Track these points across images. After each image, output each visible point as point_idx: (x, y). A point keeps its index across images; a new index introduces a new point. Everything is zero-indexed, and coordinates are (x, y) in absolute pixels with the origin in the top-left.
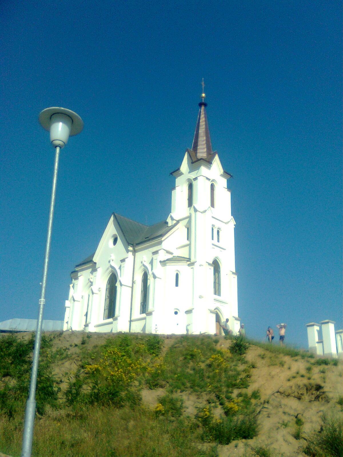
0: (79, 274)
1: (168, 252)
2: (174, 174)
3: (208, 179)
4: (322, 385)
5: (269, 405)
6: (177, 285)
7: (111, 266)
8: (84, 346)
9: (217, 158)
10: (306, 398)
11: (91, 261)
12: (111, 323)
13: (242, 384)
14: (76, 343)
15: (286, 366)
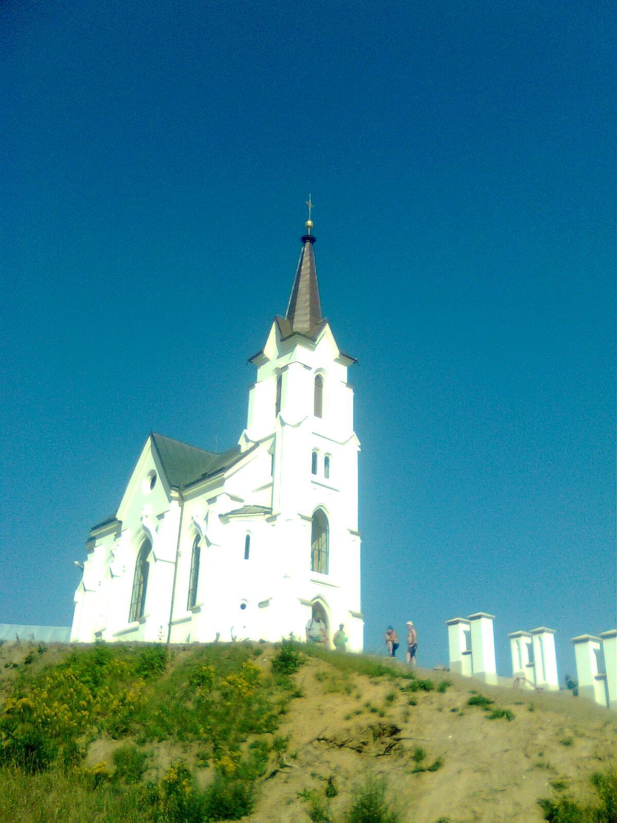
0: (98, 542)
1: (233, 498)
2: (254, 361)
3: (307, 367)
4: (400, 725)
5: (296, 761)
6: (247, 557)
7: (145, 528)
8: (29, 666)
9: (327, 329)
10: (373, 748)
11: (112, 520)
12: (136, 629)
13: (266, 726)
14: (15, 661)
15: (354, 693)
